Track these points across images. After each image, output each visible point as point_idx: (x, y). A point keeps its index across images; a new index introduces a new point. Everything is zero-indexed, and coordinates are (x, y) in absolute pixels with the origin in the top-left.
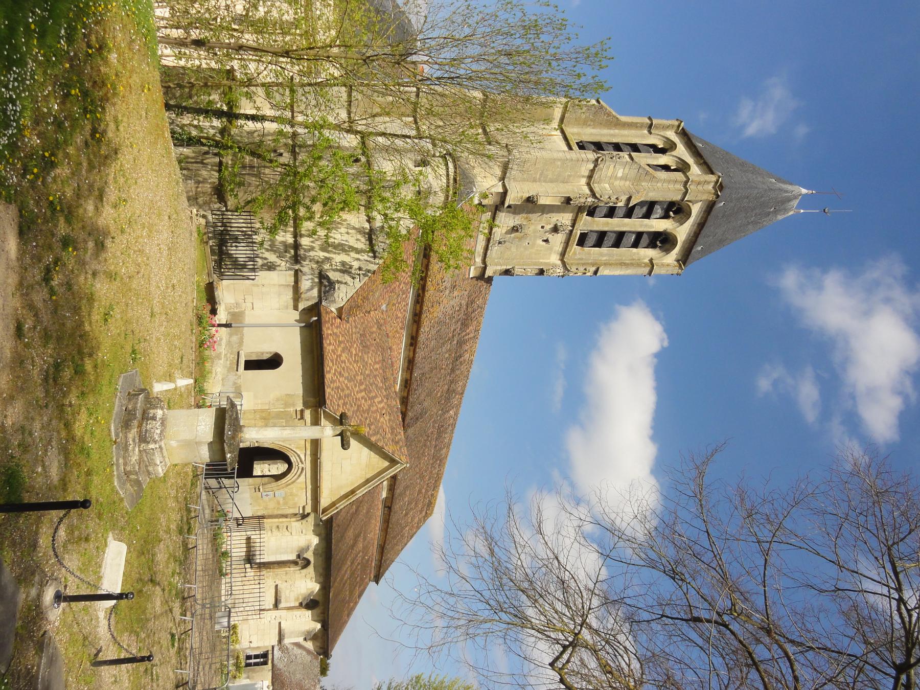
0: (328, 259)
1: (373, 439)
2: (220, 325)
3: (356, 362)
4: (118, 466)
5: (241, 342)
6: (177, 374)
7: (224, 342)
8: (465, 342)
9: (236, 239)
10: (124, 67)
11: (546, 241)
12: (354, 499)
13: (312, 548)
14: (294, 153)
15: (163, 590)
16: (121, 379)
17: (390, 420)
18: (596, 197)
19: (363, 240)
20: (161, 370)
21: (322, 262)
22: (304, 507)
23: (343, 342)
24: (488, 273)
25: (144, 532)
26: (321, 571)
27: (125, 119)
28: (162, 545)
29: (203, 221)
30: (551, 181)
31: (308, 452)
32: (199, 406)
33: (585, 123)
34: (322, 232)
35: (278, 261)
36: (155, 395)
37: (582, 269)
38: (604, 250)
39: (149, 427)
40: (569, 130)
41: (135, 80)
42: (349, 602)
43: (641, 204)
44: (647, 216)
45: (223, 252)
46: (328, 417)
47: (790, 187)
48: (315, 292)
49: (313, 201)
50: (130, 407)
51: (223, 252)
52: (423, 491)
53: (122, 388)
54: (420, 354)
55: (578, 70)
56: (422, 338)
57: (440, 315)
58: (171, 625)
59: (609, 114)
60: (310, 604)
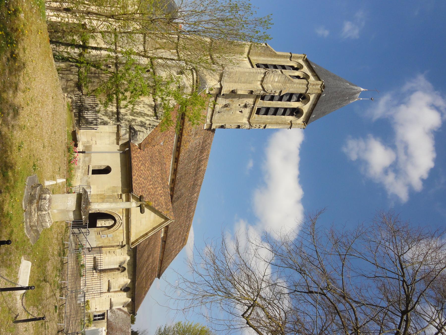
0: (134, 120)
1: (157, 208)
2: (79, 152)
4: (26, 223)
5: (90, 161)
6: (57, 176)
7: (81, 161)
8: (202, 161)
9: (87, 109)
10: (28, 21)
11: (241, 112)
12: (147, 237)
13: (126, 262)
14: (116, 66)
15: (51, 284)
16: (28, 179)
17: (165, 199)
19: (151, 110)
20: (49, 175)
21: (131, 121)
22: (122, 242)
23: (142, 160)
24: (213, 127)
25: (40, 256)
26: (131, 273)
27: (29, 48)
28: (50, 262)
29: (70, 100)
30: (244, 83)
31: (124, 215)
32: (68, 193)
33: (260, 55)
34: (130, 106)
35: (109, 120)
36: (46, 187)
37: (258, 125)
38: (269, 116)
39: (42, 203)
40: (252, 58)
41: (34, 28)
42: (145, 288)
43: (286, 94)
44: (289, 100)
45: (80, 116)
46: (134, 197)
47: (356, 88)
48: (127, 136)
49: (126, 90)
50: (32, 193)
51: (80, 116)
52: (182, 233)
54: (180, 166)
56: (181, 158)
57: (189, 147)
58: (55, 301)
59: (271, 51)
60: (126, 289)
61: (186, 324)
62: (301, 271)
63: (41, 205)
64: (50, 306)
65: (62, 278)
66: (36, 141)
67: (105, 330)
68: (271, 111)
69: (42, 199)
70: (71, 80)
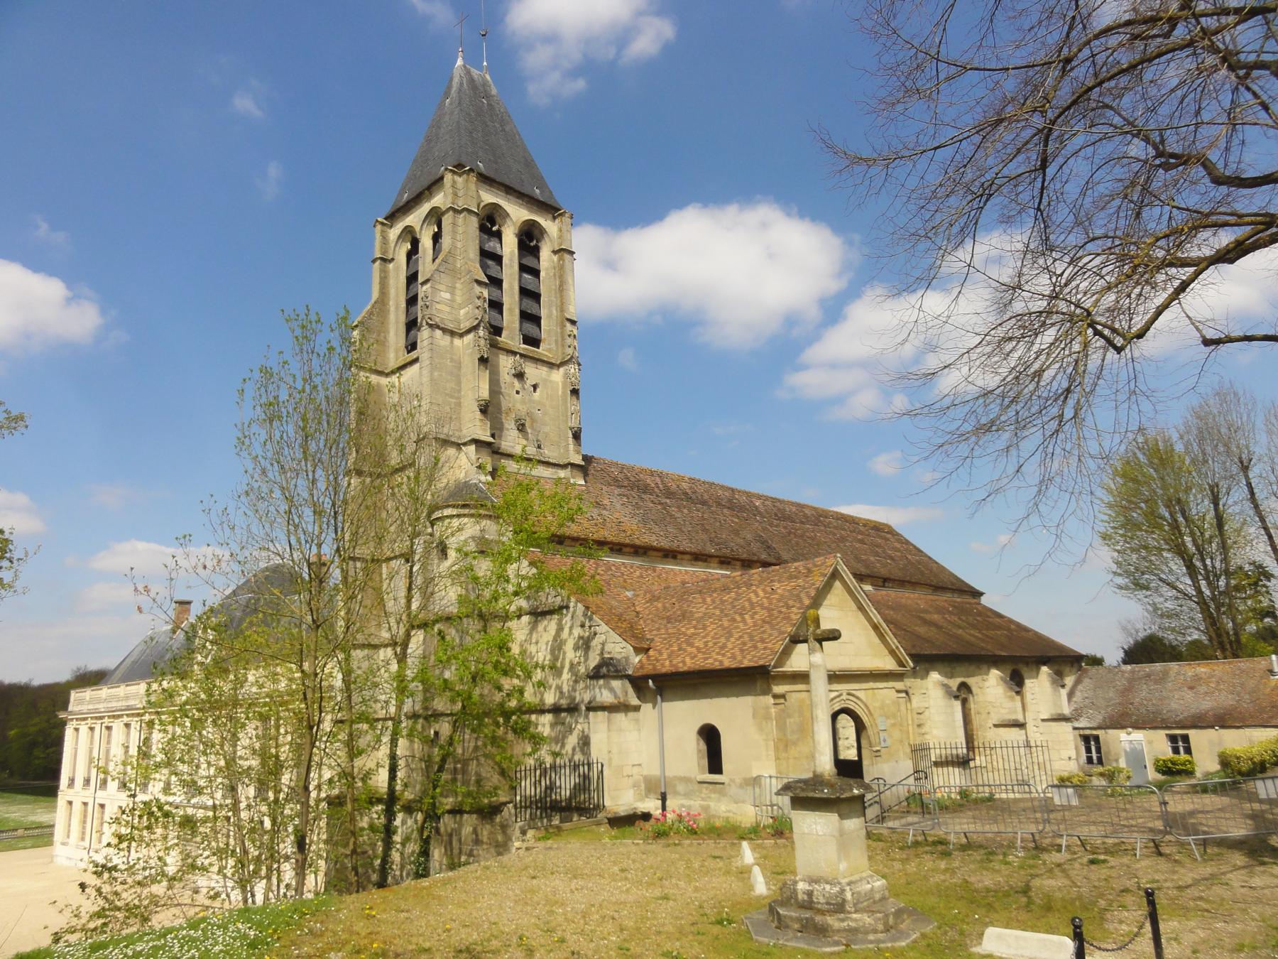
2: (664, 808)
3: (705, 627)
4: (878, 941)
5: (686, 780)
6: (737, 863)
7: (686, 802)
8: (667, 489)
9: (551, 788)
10: (346, 943)
11: (535, 387)
12: (884, 625)
13: (946, 681)
14: (437, 716)
15: (1034, 876)
17: (779, 581)
18: (478, 325)
19: (546, 622)
20: (736, 886)
22: (898, 691)
23: (679, 645)
24: (578, 460)
26: (972, 668)
27: (414, 940)
28: (973, 879)
29: (530, 833)
30: (459, 383)
33: (382, 343)
34: (538, 675)
35: (575, 733)
37: (569, 341)
38: (544, 313)
39: (822, 900)
40: (393, 360)
41: (360, 926)
42: (1009, 630)
43: (484, 267)
44: (498, 259)
47: (456, 80)
48: (616, 684)
49: (500, 689)
50: (796, 926)
51: (570, 806)
53: (772, 937)
54: (686, 545)
55: (323, 350)
56: (665, 544)
57: (635, 521)
58: (1077, 865)
59: (370, 313)
60: (1016, 681)
61: (1106, 518)
62: (986, 194)
63: (828, 903)
64: (1093, 876)
65: (1009, 847)
66: (655, 918)
67: (1129, 734)
68: (530, 306)
69: (812, 902)
70: (475, 831)
